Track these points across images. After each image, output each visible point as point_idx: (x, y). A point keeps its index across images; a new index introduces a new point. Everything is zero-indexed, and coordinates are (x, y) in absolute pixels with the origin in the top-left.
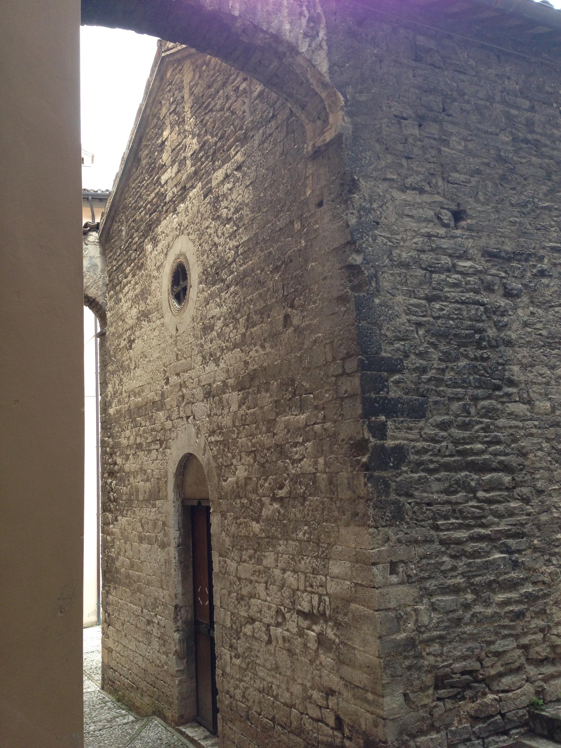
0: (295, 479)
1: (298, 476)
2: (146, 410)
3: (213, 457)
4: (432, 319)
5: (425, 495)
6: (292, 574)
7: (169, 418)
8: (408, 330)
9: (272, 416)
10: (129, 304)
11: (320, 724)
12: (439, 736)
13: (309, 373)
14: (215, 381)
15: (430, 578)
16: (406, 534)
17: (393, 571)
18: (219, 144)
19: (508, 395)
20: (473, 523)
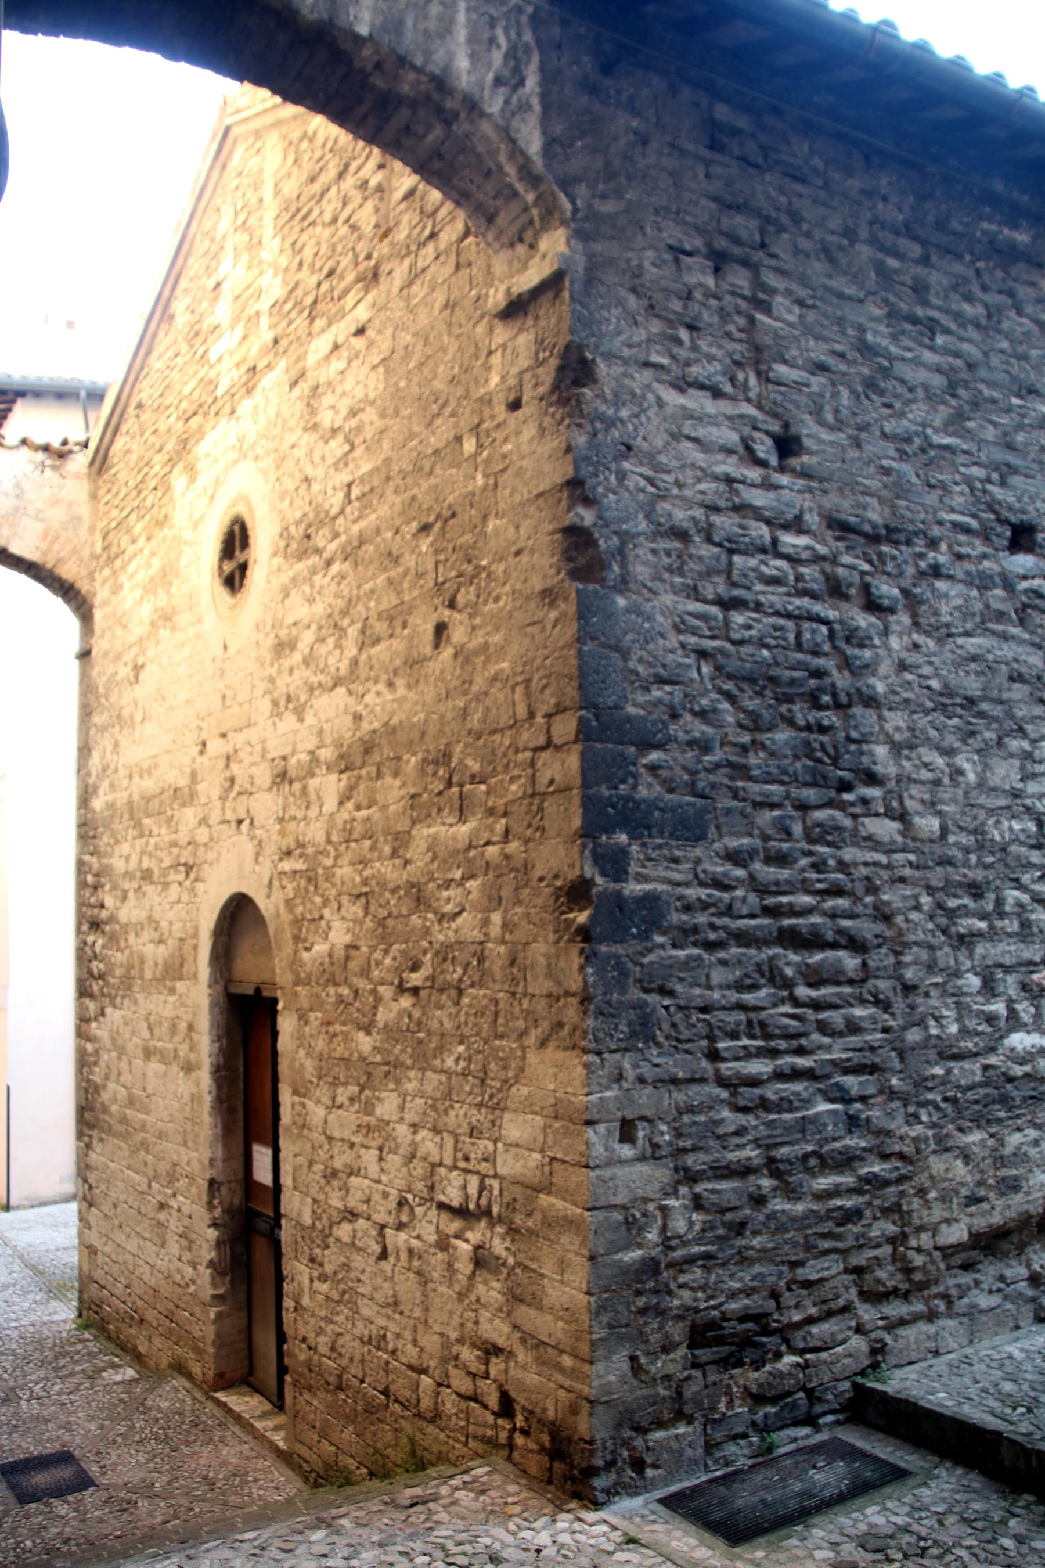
0: (444, 954)
1: (448, 947)
2: (161, 803)
3: (287, 902)
4: (728, 646)
5: (697, 991)
6: (430, 1135)
7: (203, 821)
8: (680, 665)
9: (402, 826)
10: (138, 593)
11: (473, 1404)
12: (690, 1429)
13: (481, 742)
14: (294, 752)
15: (695, 1149)
16: (656, 1066)
17: (627, 1134)
18: (325, 287)
19: (865, 801)
20: (783, 1044)
